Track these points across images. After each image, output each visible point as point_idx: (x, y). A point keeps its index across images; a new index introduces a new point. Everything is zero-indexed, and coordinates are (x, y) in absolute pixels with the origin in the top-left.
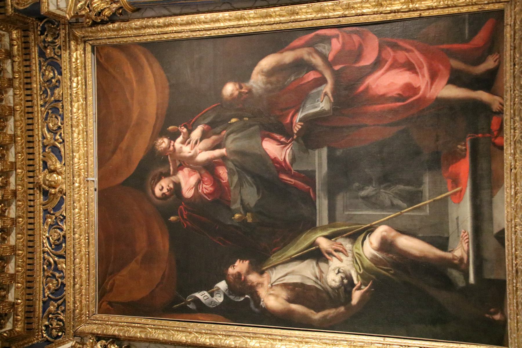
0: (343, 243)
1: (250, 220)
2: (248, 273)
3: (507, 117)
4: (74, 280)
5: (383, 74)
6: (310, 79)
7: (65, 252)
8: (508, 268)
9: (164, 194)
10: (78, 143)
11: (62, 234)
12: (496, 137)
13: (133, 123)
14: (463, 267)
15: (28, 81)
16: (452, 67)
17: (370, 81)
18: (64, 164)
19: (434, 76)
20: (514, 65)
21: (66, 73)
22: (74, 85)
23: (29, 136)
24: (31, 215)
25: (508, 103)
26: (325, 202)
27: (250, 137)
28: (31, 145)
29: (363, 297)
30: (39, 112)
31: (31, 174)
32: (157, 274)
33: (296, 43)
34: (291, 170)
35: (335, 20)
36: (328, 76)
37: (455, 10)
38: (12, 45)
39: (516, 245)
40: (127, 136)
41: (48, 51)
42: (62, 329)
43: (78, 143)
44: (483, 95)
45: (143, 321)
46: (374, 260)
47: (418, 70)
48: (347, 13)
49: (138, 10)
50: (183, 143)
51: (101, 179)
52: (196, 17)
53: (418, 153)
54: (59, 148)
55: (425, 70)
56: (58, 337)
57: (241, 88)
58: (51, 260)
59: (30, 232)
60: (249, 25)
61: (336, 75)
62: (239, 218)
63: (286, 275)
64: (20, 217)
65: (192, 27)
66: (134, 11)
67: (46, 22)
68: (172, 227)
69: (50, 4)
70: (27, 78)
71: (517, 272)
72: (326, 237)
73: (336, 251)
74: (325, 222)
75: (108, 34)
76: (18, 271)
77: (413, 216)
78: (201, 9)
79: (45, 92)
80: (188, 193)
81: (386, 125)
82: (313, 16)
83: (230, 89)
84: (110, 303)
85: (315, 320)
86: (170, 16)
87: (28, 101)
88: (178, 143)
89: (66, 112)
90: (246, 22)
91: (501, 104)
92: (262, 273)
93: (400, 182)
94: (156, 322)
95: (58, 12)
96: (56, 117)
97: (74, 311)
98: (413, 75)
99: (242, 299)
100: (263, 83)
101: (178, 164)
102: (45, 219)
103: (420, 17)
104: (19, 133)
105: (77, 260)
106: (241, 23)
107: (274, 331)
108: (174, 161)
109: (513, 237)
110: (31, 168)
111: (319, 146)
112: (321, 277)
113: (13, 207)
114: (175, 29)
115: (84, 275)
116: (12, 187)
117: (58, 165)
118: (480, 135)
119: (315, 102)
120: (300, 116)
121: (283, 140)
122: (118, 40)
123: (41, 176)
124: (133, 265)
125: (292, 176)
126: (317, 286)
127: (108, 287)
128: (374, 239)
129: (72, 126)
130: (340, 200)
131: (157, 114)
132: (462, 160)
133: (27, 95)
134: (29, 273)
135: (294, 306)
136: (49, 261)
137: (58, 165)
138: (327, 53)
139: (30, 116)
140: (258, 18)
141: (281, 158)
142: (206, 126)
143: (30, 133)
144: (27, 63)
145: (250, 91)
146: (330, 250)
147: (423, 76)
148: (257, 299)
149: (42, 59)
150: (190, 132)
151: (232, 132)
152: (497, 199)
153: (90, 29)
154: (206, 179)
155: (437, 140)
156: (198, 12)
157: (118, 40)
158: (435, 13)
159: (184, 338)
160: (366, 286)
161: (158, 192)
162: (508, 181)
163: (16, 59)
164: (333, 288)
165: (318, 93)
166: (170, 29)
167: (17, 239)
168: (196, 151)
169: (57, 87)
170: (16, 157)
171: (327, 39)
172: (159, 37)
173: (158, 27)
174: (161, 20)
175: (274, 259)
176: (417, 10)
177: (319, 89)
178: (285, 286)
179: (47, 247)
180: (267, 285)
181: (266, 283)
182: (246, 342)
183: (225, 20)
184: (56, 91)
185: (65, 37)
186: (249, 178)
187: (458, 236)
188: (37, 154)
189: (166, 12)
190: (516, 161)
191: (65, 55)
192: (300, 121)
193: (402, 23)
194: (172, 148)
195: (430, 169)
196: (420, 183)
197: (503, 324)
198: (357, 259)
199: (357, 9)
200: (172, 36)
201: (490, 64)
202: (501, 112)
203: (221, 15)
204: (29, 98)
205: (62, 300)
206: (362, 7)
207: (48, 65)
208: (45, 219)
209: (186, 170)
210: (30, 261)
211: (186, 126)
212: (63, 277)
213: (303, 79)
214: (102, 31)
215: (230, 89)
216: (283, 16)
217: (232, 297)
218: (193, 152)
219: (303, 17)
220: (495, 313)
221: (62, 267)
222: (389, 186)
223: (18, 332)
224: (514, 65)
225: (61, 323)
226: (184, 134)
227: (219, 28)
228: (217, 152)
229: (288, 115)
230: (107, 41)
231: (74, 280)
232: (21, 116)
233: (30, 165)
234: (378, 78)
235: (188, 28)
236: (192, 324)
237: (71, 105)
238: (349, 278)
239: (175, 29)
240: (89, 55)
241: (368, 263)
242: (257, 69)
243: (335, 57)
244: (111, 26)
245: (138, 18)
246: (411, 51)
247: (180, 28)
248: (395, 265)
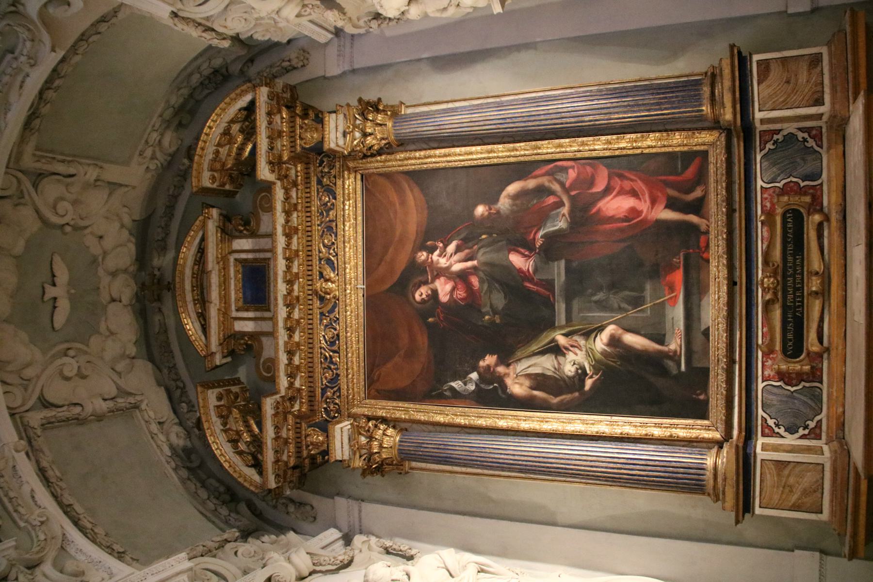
0: (578, 340)
1: (498, 321)
2: (497, 365)
3: (712, 236)
4: (347, 371)
5: (612, 199)
6: (550, 202)
7: (339, 348)
8: (712, 358)
9: (423, 299)
10: (350, 257)
11: (336, 332)
12: (704, 253)
13: (396, 239)
14: (676, 358)
15: (308, 205)
16: (668, 195)
17: (601, 204)
18: (338, 274)
19: (653, 202)
20: (717, 195)
21: (340, 198)
22: (347, 207)
23: (309, 251)
24: (310, 317)
25: (713, 225)
26: (563, 306)
27: (498, 250)
28: (310, 258)
29: (594, 383)
30: (317, 230)
31: (310, 283)
32: (418, 367)
33: (538, 172)
34: (533, 279)
35: (571, 154)
36: (565, 199)
37: (670, 149)
38: (297, 176)
39: (718, 339)
40: (391, 250)
41: (325, 180)
42: (338, 411)
43: (350, 257)
44: (693, 218)
45: (406, 405)
46: (604, 353)
47: (641, 196)
48: (581, 148)
49: (402, 145)
50: (440, 256)
51: (369, 287)
52: (453, 150)
53: (641, 265)
54: (332, 261)
55: (647, 197)
56: (335, 417)
57: (490, 209)
58: (327, 354)
59: (310, 331)
60: (498, 157)
61: (572, 199)
62: (489, 319)
63: (529, 367)
64: (302, 319)
65: (449, 159)
66: (398, 146)
67: (324, 156)
68: (429, 326)
69: (331, 142)
70: (307, 202)
71: (718, 361)
72: (563, 335)
73: (572, 346)
74: (563, 322)
75: (376, 165)
76: (301, 363)
77: (637, 317)
78: (456, 144)
79: (322, 214)
80: (444, 298)
81: (614, 242)
82: (553, 150)
83: (480, 210)
84: (377, 391)
85: (554, 404)
86: (430, 149)
87: (308, 222)
88: (435, 256)
89: (339, 230)
90: (496, 155)
91: (707, 225)
92: (508, 365)
93: (626, 288)
94: (418, 406)
95: (338, 149)
96: (331, 235)
97: (347, 397)
98: (637, 201)
99: (491, 387)
100: (510, 205)
101: (435, 273)
102: (321, 320)
103: (642, 154)
104: (301, 248)
105: (350, 355)
106: (491, 155)
107: (519, 413)
108: (432, 271)
109: (716, 333)
110: (310, 278)
111: (558, 259)
112: (559, 368)
113: (297, 310)
114: (433, 160)
115: (355, 368)
116: (296, 293)
117: (332, 275)
118: (691, 251)
119: (554, 221)
120: (541, 233)
121: (527, 253)
122: (384, 169)
123: (319, 285)
124: (397, 359)
125: (535, 284)
126: (555, 375)
127: (375, 378)
128: (605, 336)
129: (344, 242)
130: (576, 304)
131: (417, 231)
132: (677, 271)
133: (307, 217)
134: (310, 365)
135: (536, 393)
136: (325, 356)
137: (332, 275)
138: (565, 180)
139: (309, 234)
140: (506, 151)
141: (525, 269)
142: (460, 242)
143: (309, 248)
144: (308, 190)
145: (498, 212)
146: (567, 345)
147: (645, 201)
148: (504, 387)
149: (319, 187)
150: (446, 246)
151: (482, 247)
152: (704, 303)
153: (361, 161)
154: (460, 286)
155: (657, 255)
156: (454, 146)
157: (384, 169)
158: (654, 150)
159: (442, 419)
160: (597, 375)
161: (417, 297)
162: (713, 287)
163: (299, 187)
164: (569, 378)
165: (557, 215)
166: (429, 160)
167: (301, 336)
168: (451, 263)
169: (331, 209)
170: (299, 269)
171: (565, 169)
172: (419, 166)
173: (419, 158)
174: (422, 153)
175: (519, 354)
176: (639, 148)
177: (558, 210)
178: (528, 376)
179: (324, 344)
180: (512, 375)
181: (512, 374)
182: (496, 422)
183: (477, 153)
184: (331, 213)
185: (339, 168)
186: (497, 285)
187: (673, 333)
188: (314, 266)
189: (425, 146)
190: (719, 272)
191: (339, 183)
192: (542, 237)
193: (627, 158)
194: (430, 260)
195: (651, 278)
196: (642, 290)
197: (706, 402)
198: (589, 353)
199: (590, 145)
200: (431, 165)
201: (698, 193)
202: (707, 232)
203: (473, 149)
204: (309, 219)
205: (337, 388)
206: (594, 144)
207: (324, 191)
208: (321, 320)
209: (442, 279)
210: (311, 355)
211: (442, 242)
212: (337, 369)
213: (544, 202)
214: (370, 163)
215: (480, 210)
216: (527, 150)
217: (482, 386)
218: (448, 263)
219: (545, 151)
220: (700, 394)
221: (336, 361)
222: (617, 292)
223: (304, 412)
224: (717, 195)
225: (337, 406)
226: (441, 248)
227: (472, 160)
228: (469, 264)
229: (531, 232)
230: (375, 171)
231: (347, 371)
232: (303, 234)
233: (309, 275)
234: (608, 202)
235: (445, 159)
236: (448, 408)
237: (344, 224)
238: (583, 369)
239: (433, 160)
240: (359, 182)
241: (598, 356)
242: (504, 193)
243: (571, 185)
244: (379, 158)
245: (402, 152)
246: (636, 181)
247: (438, 160)
248: (621, 357)
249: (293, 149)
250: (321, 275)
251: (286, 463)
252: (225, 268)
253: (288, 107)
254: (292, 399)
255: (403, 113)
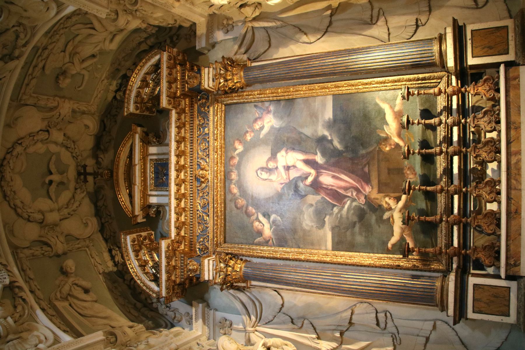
249: (183, 89)
250: (199, 165)
251: (174, 281)
252: (145, 164)
253: (181, 65)
254: (179, 242)
255: (249, 66)
